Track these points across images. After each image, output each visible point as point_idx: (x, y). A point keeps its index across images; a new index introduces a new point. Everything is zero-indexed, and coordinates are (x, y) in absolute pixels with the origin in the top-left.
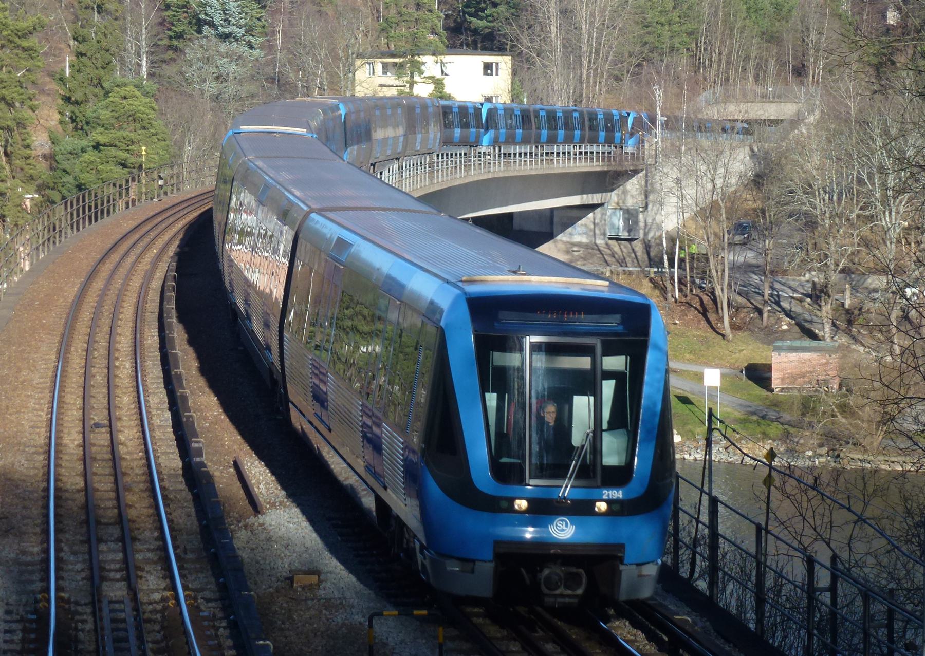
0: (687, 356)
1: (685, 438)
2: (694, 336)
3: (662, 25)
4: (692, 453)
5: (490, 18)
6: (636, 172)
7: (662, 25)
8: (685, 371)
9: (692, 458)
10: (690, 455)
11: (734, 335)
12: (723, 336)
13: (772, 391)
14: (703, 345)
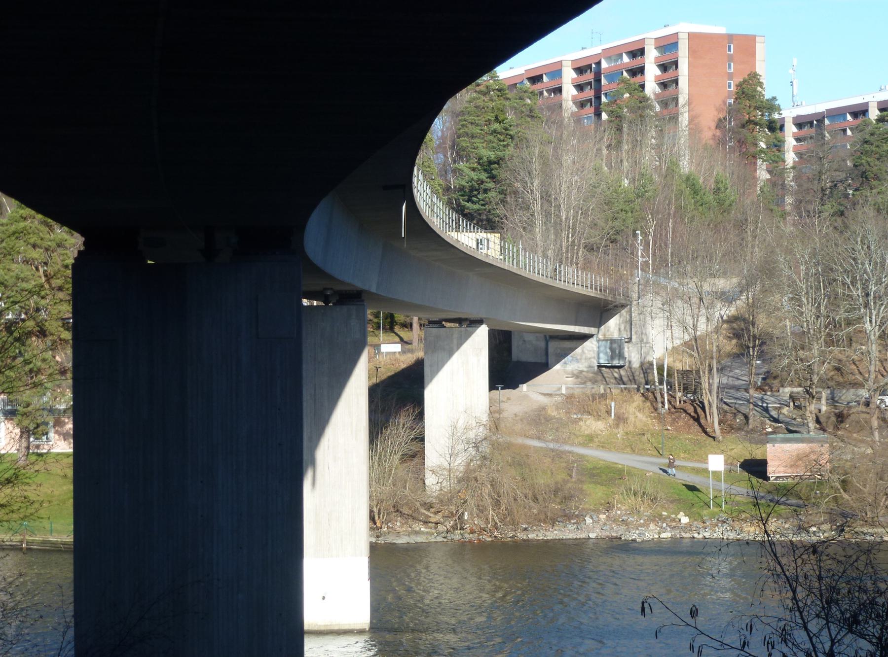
0: (682, 455)
1: (692, 519)
2: (686, 439)
3: (626, 212)
4: (701, 532)
5: (483, 202)
6: (623, 306)
7: (626, 212)
8: (682, 466)
9: (701, 536)
10: (699, 534)
11: (724, 437)
12: (714, 438)
13: (766, 478)
14: (695, 446)
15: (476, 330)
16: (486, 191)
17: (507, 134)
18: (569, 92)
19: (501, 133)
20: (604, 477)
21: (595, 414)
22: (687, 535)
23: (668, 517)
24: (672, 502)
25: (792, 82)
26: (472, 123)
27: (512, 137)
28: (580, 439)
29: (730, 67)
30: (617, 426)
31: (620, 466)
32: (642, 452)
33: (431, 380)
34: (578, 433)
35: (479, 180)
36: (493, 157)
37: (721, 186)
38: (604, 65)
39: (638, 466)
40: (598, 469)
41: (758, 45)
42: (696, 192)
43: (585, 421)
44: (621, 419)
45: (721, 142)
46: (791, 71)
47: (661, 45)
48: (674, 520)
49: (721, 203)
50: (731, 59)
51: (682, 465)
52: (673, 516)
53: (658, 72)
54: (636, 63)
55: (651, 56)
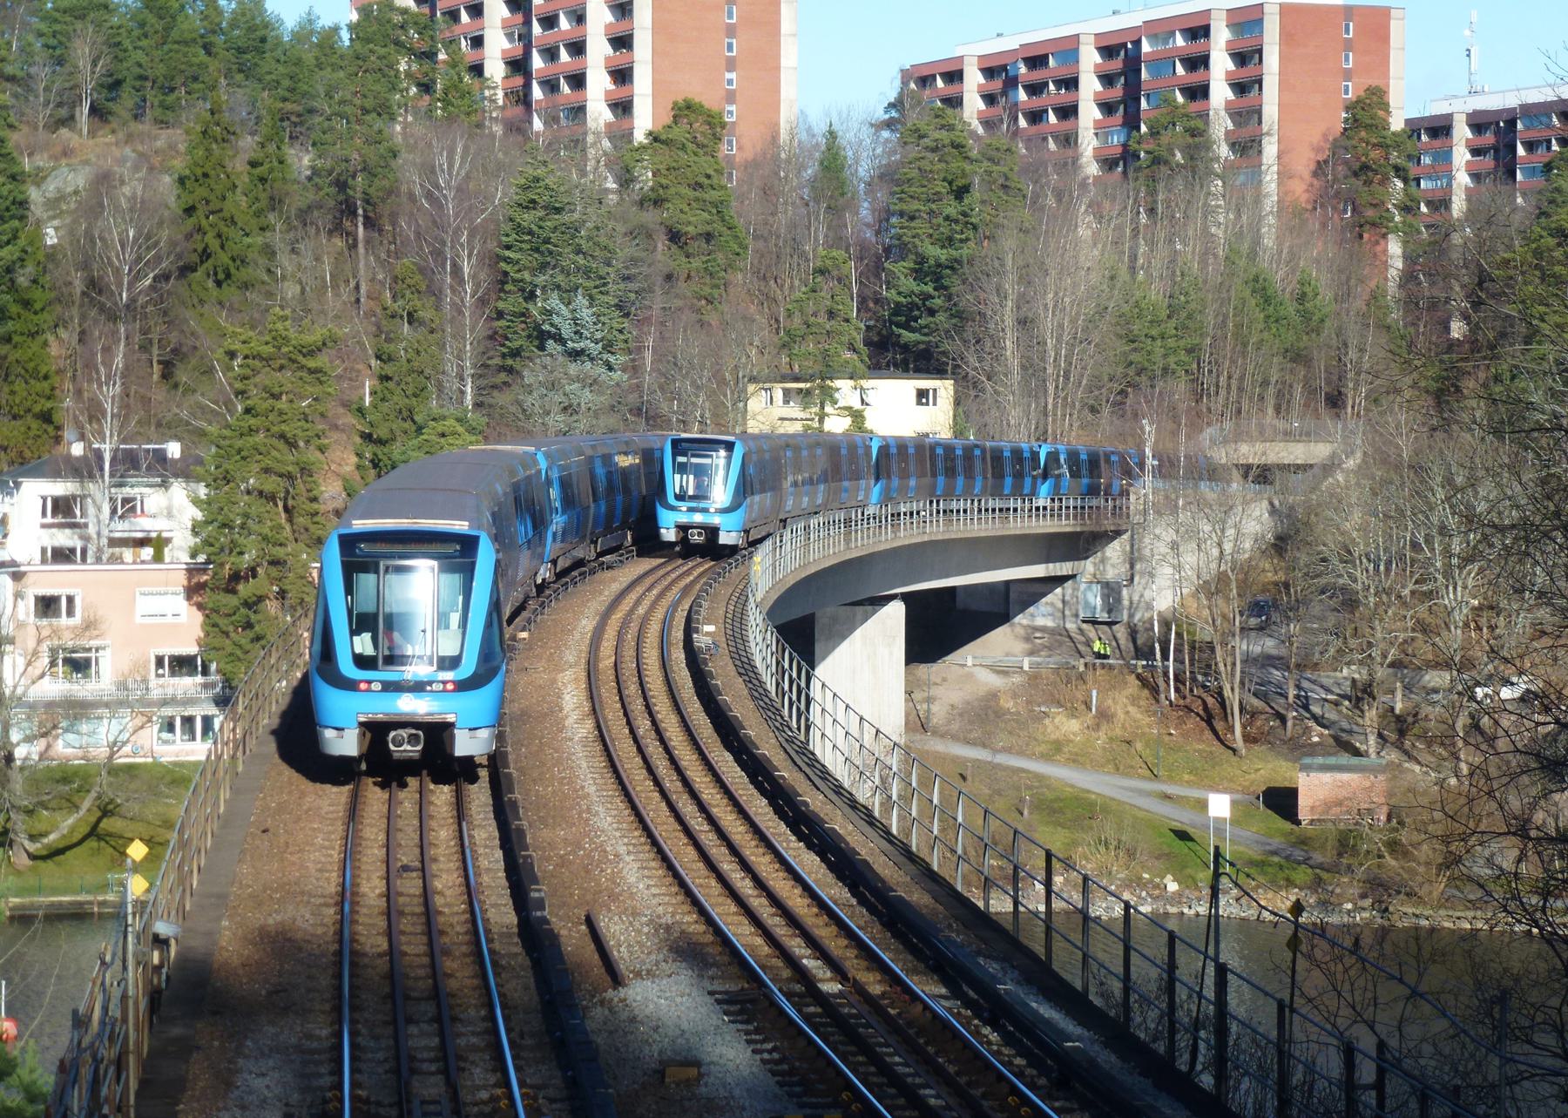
0: (1186, 777)
2: (1195, 751)
3: (1153, 339)
5: (926, 330)
7: (1153, 339)
8: (1182, 797)
9: (1192, 912)
11: (1248, 750)
12: (1234, 750)
13: (1298, 823)
15: (875, 612)
16: (932, 312)
17: (967, 223)
18: (1090, 85)
19: (956, 221)
20: (1069, 816)
21: (1069, 705)
22: (1173, 910)
23: (1151, 881)
24: (1158, 858)
25: (1468, 50)
26: (911, 197)
27: (975, 228)
28: (1043, 748)
29: (1347, 59)
30: (1097, 727)
31: (1093, 797)
32: (1128, 772)
33: (824, 658)
34: (1041, 737)
35: (922, 293)
36: (943, 258)
37: (1308, 289)
38: (1146, 47)
39: (1118, 797)
40: (1062, 800)
41: (1393, 23)
42: (1267, 301)
43: (1053, 718)
44: (1104, 716)
45: (1319, 201)
46: (1467, 33)
47: (1236, 21)
48: (1157, 886)
49: (1306, 316)
50: (1348, 46)
51: (1182, 794)
52: (1157, 880)
53: (1231, 66)
54: (1197, 48)
55: (1221, 37)
